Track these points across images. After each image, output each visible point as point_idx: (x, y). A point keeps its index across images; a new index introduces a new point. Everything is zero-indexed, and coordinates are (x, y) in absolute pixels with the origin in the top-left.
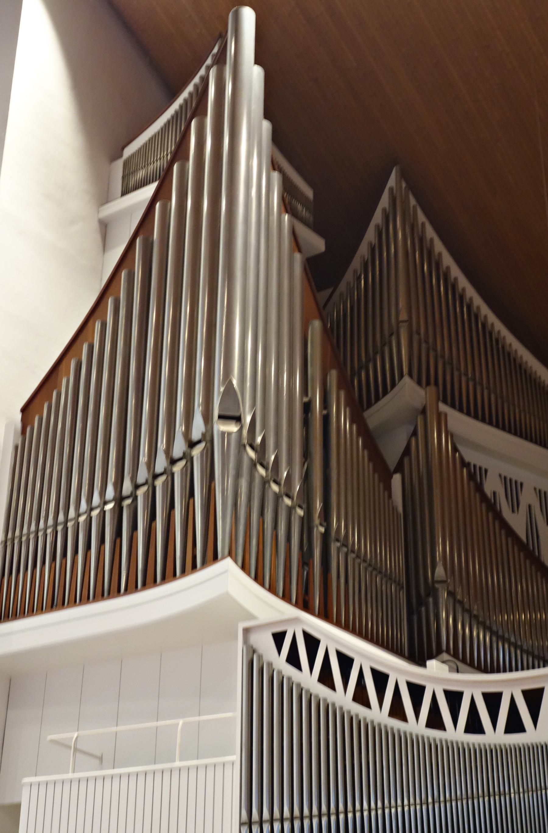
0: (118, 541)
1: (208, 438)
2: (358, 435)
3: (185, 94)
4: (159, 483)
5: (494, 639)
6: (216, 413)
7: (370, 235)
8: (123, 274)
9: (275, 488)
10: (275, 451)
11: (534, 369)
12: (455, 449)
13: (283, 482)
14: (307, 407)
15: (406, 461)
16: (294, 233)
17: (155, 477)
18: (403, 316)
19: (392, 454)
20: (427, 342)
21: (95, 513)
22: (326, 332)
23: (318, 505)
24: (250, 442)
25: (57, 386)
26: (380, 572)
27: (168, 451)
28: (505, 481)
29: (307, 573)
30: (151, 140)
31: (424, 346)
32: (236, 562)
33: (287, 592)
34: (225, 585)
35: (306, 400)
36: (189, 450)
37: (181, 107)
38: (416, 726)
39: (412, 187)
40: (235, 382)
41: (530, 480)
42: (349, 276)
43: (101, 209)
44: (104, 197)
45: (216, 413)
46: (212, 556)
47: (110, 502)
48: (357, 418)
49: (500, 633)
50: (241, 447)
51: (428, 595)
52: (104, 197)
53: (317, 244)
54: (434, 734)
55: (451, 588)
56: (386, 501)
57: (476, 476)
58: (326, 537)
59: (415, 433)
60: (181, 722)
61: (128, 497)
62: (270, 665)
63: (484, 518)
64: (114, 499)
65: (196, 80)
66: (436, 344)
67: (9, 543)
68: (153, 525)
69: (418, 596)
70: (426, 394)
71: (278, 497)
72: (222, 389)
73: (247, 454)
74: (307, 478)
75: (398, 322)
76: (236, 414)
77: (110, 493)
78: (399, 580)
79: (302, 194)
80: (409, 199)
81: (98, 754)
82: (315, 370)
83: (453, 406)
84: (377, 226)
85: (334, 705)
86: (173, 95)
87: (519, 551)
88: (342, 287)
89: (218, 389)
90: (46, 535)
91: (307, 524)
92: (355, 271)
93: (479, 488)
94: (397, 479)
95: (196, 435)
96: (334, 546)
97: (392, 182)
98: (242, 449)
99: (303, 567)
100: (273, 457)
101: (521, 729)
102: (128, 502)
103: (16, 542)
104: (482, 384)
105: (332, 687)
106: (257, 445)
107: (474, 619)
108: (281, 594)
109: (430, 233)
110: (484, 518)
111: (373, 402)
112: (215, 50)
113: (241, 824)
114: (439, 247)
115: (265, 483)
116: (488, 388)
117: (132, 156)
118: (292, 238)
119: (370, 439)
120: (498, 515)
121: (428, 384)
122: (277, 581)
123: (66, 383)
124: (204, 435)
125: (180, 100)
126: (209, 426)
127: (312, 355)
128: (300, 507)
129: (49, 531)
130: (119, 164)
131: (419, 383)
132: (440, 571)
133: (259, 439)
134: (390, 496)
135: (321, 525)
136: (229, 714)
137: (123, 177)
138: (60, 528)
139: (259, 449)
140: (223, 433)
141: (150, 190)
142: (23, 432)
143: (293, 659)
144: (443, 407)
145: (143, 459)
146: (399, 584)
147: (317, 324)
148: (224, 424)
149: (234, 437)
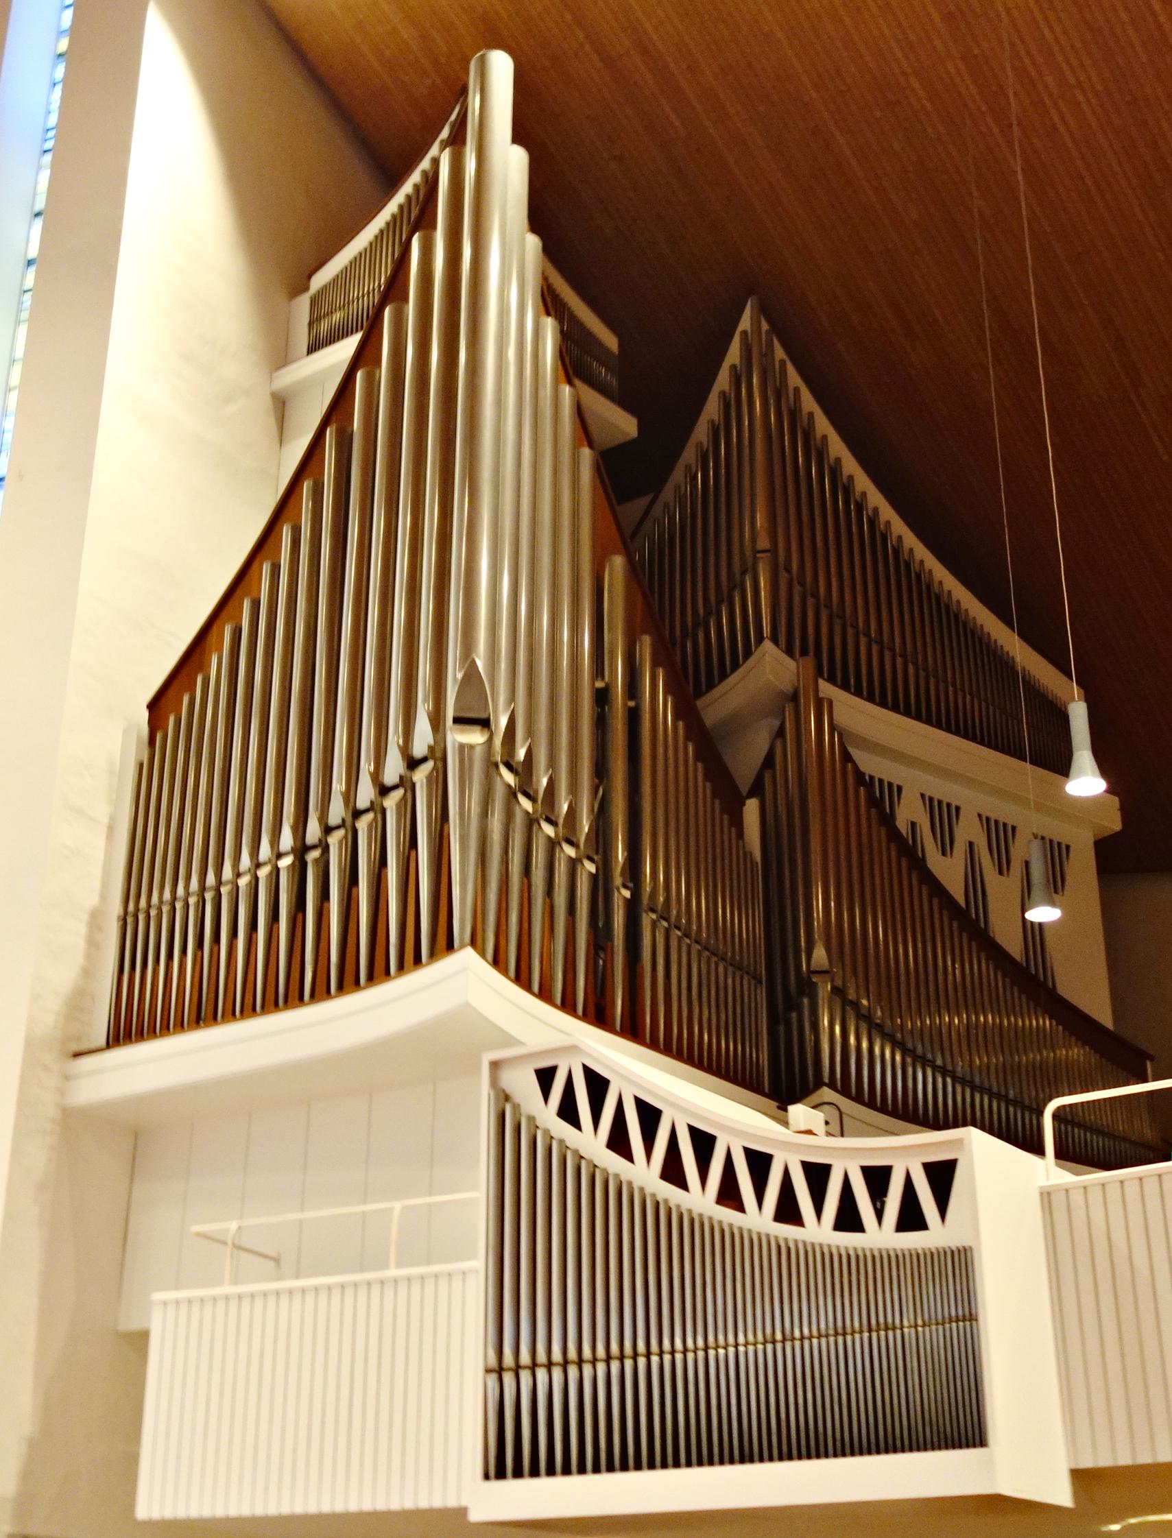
0: (300, 916)
1: (439, 754)
2: (688, 738)
3: (407, 188)
4: (363, 824)
5: (909, 1060)
6: (450, 714)
7: (712, 408)
8: (306, 486)
9: (548, 830)
10: (547, 770)
11: (972, 614)
12: (847, 757)
13: (561, 821)
14: (602, 697)
15: (767, 776)
16: (579, 411)
17: (357, 814)
18: (763, 543)
19: (744, 762)
20: (802, 583)
21: (263, 873)
22: (634, 571)
23: (621, 855)
24: (505, 759)
25: (203, 667)
26: (723, 959)
27: (376, 777)
28: (931, 803)
29: (605, 965)
30: (355, 262)
31: (797, 588)
32: (483, 955)
33: (569, 997)
34: (464, 987)
35: (599, 684)
36: (408, 773)
37: (401, 207)
38: (758, 1218)
39: (780, 330)
40: (480, 664)
41: (972, 803)
42: (678, 475)
43: (275, 375)
44: (280, 358)
45: (450, 714)
46: (445, 944)
47: (286, 854)
48: (686, 711)
49: (919, 1051)
50: (491, 767)
51: (801, 993)
52: (280, 358)
53: (622, 424)
54: (787, 1231)
55: (839, 983)
56: (734, 842)
57: (879, 798)
58: (633, 909)
59: (781, 733)
60: (397, 1206)
61: (314, 847)
62: (531, 1119)
63: (894, 865)
64: (294, 850)
65: (415, 177)
66: (817, 586)
67: (130, 920)
68: (354, 890)
69: (788, 995)
70: (798, 668)
71: (552, 844)
72: (459, 676)
73: (501, 775)
74: (602, 815)
75: (755, 552)
76: (483, 716)
77: (287, 840)
78: (755, 969)
79: (600, 344)
80: (773, 351)
81: (274, 1254)
82: (616, 638)
83: (845, 687)
84: (723, 394)
85: (630, 1184)
86: (392, 183)
87: (951, 919)
88: (668, 493)
89: (454, 674)
90: (187, 905)
91: (601, 885)
92: (688, 468)
93: (888, 820)
94: (751, 808)
95: (419, 750)
96: (647, 919)
97: (745, 323)
98: (493, 769)
99: (596, 954)
100: (545, 781)
101: (921, 1225)
102: (315, 854)
103: (141, 917)
104: (892, 649)
105: (628, 1156)
106: (518, 763)
107: (875, 1028)
108: (558, 1001)
109: (809, 403)
110: (894, 865)
111: (728, 670)
112: (453, 117)
113: (488, 1371)
114: (823, 425)
115: (531, 822)
116: (904, 656)
117: (324, 289)
118: (578, 420)
119: (707, 744)
120: (919, 864)
121: (804, 653)
122: (552, 979)
123: (217, 664)
124: (431, 749)
125: (399, 198)
126: (439, 737)
127: (610, 612)
128: (591, 859)
129: (192, 900)
130: (304, 301)
131: (789, 652)
132: (820, 955)
133: (521, 754)
134: (740, 835)
135: (625, 887)
136: (474, 1194)
137: (310, 324)
138: (209, 896)
139: (520, 770)
140: (462, 747)
141: (348, 347)
142: (152, 742)
143: (568, 1112)
144: (827, 689)
145: (339, 786)
146: (754, 978)
147: (618, 562)
148: (462, 731)
149: (478, 755)
